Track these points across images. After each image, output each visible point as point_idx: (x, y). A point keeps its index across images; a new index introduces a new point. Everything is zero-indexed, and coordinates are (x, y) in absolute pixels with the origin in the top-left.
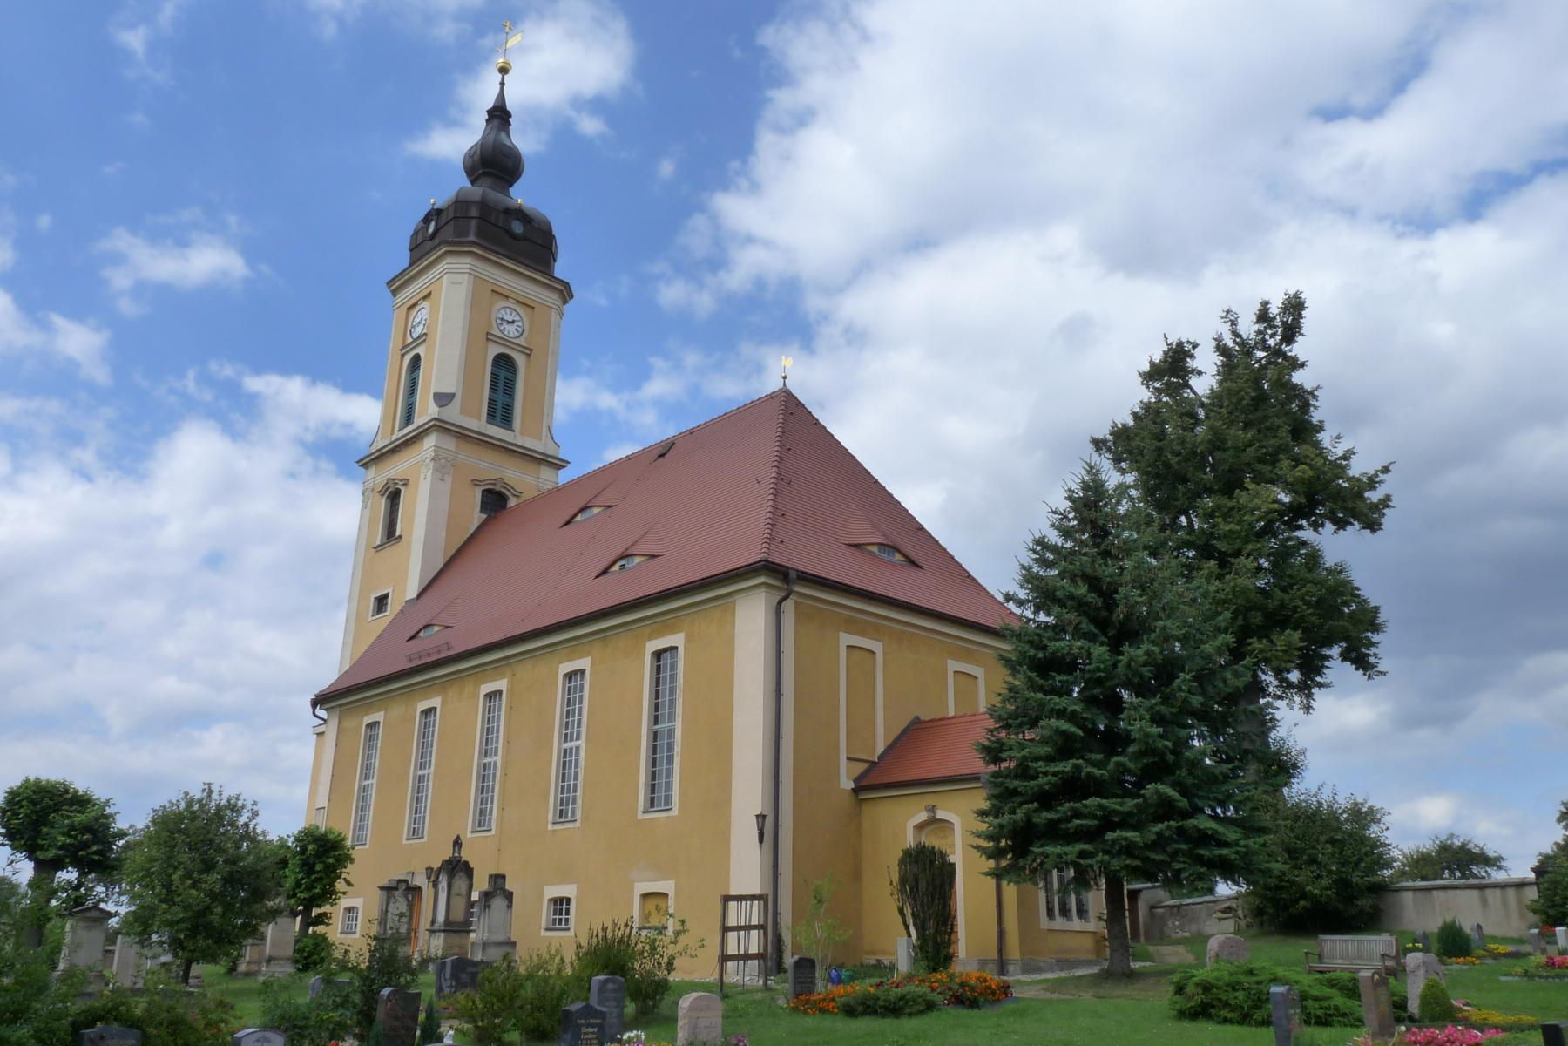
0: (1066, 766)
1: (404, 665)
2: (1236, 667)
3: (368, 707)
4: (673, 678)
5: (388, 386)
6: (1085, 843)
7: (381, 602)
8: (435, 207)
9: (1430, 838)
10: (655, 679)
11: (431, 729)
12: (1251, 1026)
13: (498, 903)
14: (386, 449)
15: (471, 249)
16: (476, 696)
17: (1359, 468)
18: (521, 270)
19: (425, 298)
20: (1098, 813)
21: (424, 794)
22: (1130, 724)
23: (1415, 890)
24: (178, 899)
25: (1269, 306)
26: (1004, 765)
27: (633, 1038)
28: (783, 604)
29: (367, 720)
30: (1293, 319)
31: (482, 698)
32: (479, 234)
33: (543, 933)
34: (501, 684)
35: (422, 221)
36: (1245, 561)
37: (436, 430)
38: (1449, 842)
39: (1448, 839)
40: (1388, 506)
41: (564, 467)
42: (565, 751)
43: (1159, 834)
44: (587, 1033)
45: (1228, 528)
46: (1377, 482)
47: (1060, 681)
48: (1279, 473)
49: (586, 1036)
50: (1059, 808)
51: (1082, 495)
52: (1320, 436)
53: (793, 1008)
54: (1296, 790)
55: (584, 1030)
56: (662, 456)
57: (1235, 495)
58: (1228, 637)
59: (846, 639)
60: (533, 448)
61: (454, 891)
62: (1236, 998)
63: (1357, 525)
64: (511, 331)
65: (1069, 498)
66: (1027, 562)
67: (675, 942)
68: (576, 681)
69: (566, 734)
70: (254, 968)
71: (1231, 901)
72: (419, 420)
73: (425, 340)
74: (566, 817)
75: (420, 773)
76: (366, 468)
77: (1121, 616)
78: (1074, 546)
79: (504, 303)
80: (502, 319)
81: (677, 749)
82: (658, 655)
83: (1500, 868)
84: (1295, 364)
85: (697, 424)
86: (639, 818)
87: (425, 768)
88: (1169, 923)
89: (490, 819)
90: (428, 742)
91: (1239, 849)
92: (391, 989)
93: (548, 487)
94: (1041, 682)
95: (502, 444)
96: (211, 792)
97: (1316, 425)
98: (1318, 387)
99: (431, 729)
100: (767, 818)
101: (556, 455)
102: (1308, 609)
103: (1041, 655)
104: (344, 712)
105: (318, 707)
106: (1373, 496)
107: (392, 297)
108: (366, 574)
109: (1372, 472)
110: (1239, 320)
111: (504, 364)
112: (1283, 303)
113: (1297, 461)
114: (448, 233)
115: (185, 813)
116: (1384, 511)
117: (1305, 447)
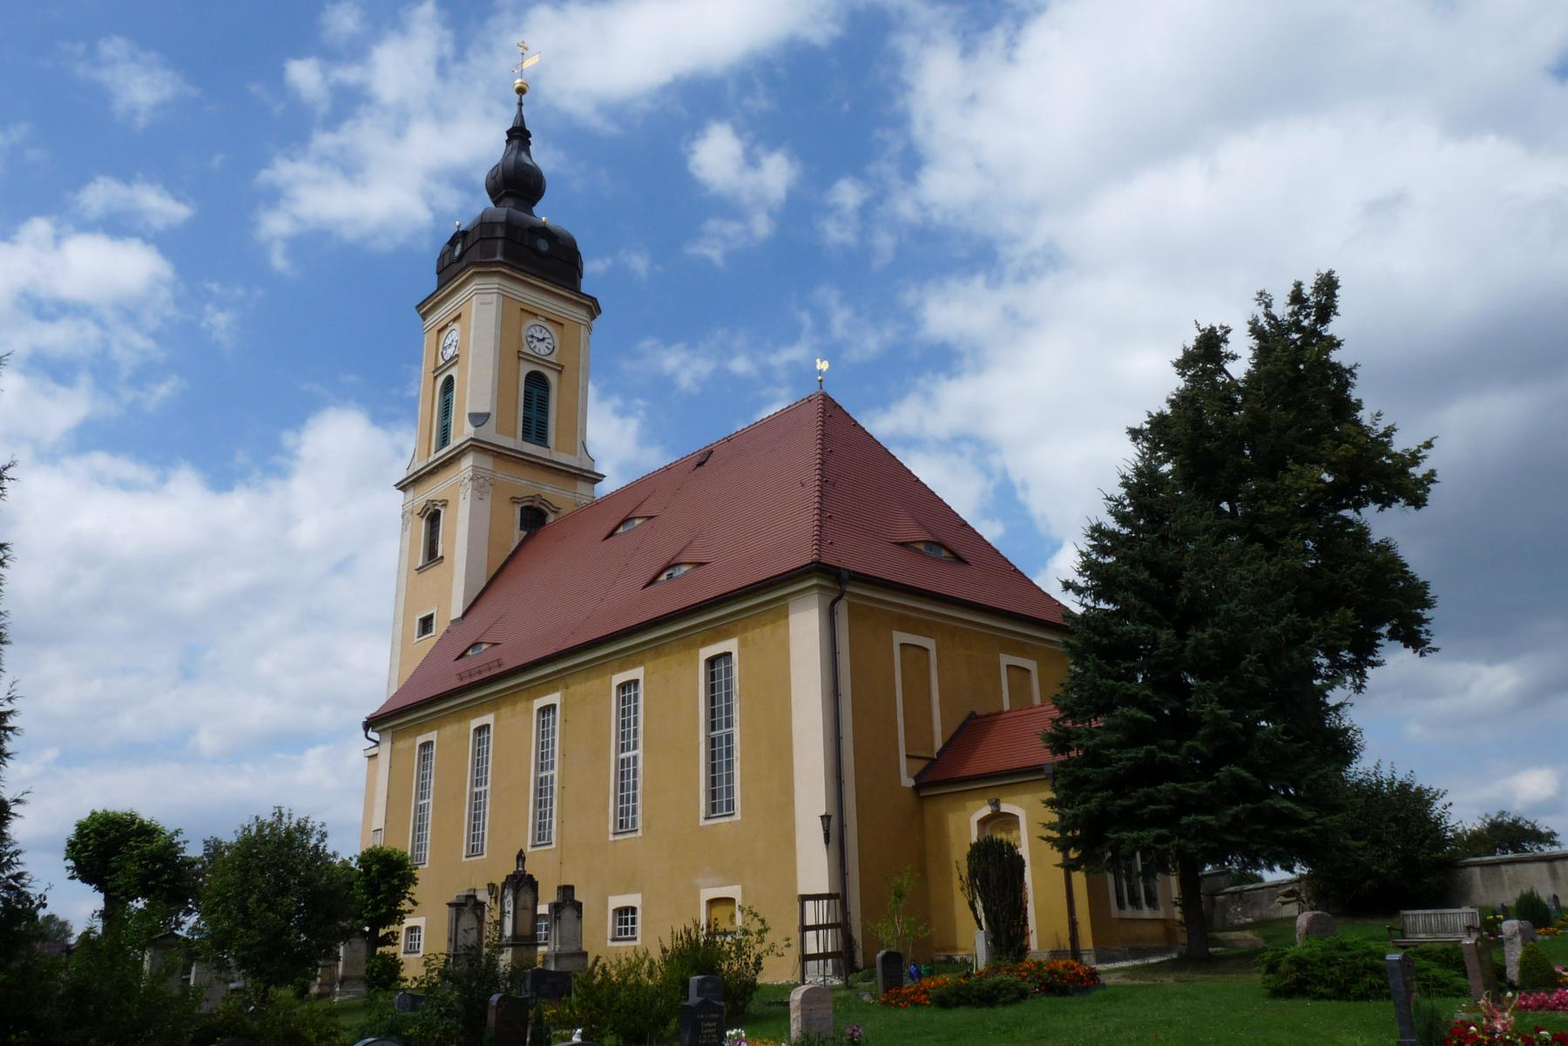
0: (1140, 753)
1: (455, 683)
2: (1303, 645)
3: (421, 727)
4: (729, 685)
5: (422, 408)
6: (1161, 829)
7: (426, 624)
8: (461, 230)
9: (1479, 818)
10: (709, 687)
11: (485, 746)
12: (1349, 1000)
13: (568, 914)
14: (422, 473)
15: (499, 269)
16: (529, 711)
17: (1401, 444)
18: (540, 284)
19: (456, 319)
20: (1173, 798)
21: (482, 811)
22: (1199, 707)
23: (1482, 865)
24: (254, 923)
25: (1302, 287)
26: (1073, 754)
27: (734, 1036)
28: (837, 604)
29: (421, 739)
30: (1326, 299)
31: (535, 712)
32: (505, 254)
33: (610, 944)
34: (554, 698)
35: (448, 243)
36: (1291, 541)
37: (473, 450)
38: (1500, 819)
39: (1499, 817)
40: (1433, 481)
41: (600, 481)
42: (623, 760)
43: (1234, 816)
44: (706, 1028)
45: (1273, 510)
46: (1421, 458)
47: (1124, 668)
48: (1321, 453)
49: (706, 1031)
50: (1133, 794)
51: (1136, 481)
52: (1360, 414)
53: (884, 1003)
54: (1353, 770)
55: (704, 1025)
56: (700, 464)
57: (1279, 476)
58: (1293, 616)
59: (900, 637)
60: (568, 463)
61: (520, 906)
62: (1332, 973)
63: (1402, 501)
64: (542, 348)
65: (1124, 485)
66: (1085, 549)
67: (762, 941)
68: (630, 691)
69: (623, 745)
70: (326, 989)
71: (1294, 885)
72: (455, 441)
73: (457, 361)
74: (627, 826)
75: (476, 790)
76: (405, 491)
77: (1185, 600)
78: (1131, 533)
79: (534, 321)
80: (532, 336)
81: (737, 754)
82: (712, 662)
83: (1553, 843)
84: (1334, 344)
85: (722, 437)
86: (701, 824)
87: (481, 785)
88: (1231, 909)
89: (550, 833)
90: (483, 758)
91: (1316, 827)
92: (500, 995)
93: (586, 501)
94: (1108, 669)
95: (539, 461)
96: (281, 815)
97: (1355, 404)
98: (1356, 366)
99: (485, 746)
100: (832, 818)
101: (591, 469)
102: (1358, 587)
103: (1105, 641)
104: (397, 734)
105: (370, 729)
106: (1418, 472)
107: (421, 320)
108: (410, 597)
109: (1414, 448)
110: (1273, 302)
111: (537, 385)
112: (1316, 283)
113: (1339, 439)
114: (475, 254)
115: (257, 838)
116: (1429, 486)
117: (1346, 426)
